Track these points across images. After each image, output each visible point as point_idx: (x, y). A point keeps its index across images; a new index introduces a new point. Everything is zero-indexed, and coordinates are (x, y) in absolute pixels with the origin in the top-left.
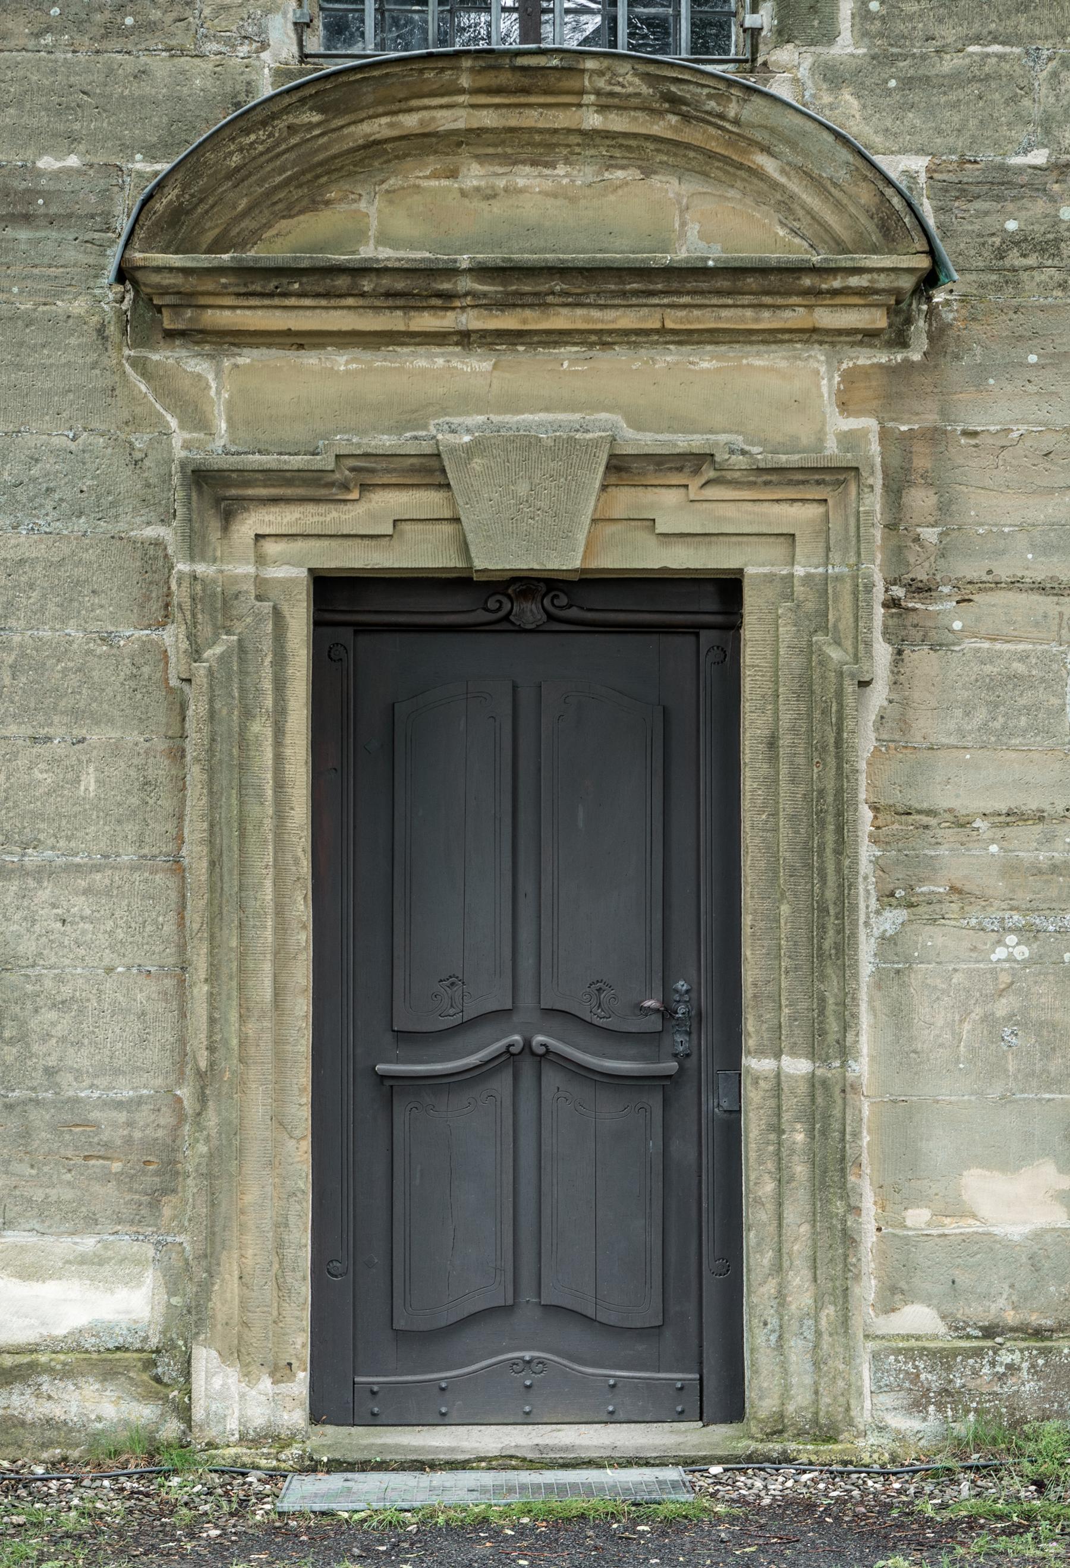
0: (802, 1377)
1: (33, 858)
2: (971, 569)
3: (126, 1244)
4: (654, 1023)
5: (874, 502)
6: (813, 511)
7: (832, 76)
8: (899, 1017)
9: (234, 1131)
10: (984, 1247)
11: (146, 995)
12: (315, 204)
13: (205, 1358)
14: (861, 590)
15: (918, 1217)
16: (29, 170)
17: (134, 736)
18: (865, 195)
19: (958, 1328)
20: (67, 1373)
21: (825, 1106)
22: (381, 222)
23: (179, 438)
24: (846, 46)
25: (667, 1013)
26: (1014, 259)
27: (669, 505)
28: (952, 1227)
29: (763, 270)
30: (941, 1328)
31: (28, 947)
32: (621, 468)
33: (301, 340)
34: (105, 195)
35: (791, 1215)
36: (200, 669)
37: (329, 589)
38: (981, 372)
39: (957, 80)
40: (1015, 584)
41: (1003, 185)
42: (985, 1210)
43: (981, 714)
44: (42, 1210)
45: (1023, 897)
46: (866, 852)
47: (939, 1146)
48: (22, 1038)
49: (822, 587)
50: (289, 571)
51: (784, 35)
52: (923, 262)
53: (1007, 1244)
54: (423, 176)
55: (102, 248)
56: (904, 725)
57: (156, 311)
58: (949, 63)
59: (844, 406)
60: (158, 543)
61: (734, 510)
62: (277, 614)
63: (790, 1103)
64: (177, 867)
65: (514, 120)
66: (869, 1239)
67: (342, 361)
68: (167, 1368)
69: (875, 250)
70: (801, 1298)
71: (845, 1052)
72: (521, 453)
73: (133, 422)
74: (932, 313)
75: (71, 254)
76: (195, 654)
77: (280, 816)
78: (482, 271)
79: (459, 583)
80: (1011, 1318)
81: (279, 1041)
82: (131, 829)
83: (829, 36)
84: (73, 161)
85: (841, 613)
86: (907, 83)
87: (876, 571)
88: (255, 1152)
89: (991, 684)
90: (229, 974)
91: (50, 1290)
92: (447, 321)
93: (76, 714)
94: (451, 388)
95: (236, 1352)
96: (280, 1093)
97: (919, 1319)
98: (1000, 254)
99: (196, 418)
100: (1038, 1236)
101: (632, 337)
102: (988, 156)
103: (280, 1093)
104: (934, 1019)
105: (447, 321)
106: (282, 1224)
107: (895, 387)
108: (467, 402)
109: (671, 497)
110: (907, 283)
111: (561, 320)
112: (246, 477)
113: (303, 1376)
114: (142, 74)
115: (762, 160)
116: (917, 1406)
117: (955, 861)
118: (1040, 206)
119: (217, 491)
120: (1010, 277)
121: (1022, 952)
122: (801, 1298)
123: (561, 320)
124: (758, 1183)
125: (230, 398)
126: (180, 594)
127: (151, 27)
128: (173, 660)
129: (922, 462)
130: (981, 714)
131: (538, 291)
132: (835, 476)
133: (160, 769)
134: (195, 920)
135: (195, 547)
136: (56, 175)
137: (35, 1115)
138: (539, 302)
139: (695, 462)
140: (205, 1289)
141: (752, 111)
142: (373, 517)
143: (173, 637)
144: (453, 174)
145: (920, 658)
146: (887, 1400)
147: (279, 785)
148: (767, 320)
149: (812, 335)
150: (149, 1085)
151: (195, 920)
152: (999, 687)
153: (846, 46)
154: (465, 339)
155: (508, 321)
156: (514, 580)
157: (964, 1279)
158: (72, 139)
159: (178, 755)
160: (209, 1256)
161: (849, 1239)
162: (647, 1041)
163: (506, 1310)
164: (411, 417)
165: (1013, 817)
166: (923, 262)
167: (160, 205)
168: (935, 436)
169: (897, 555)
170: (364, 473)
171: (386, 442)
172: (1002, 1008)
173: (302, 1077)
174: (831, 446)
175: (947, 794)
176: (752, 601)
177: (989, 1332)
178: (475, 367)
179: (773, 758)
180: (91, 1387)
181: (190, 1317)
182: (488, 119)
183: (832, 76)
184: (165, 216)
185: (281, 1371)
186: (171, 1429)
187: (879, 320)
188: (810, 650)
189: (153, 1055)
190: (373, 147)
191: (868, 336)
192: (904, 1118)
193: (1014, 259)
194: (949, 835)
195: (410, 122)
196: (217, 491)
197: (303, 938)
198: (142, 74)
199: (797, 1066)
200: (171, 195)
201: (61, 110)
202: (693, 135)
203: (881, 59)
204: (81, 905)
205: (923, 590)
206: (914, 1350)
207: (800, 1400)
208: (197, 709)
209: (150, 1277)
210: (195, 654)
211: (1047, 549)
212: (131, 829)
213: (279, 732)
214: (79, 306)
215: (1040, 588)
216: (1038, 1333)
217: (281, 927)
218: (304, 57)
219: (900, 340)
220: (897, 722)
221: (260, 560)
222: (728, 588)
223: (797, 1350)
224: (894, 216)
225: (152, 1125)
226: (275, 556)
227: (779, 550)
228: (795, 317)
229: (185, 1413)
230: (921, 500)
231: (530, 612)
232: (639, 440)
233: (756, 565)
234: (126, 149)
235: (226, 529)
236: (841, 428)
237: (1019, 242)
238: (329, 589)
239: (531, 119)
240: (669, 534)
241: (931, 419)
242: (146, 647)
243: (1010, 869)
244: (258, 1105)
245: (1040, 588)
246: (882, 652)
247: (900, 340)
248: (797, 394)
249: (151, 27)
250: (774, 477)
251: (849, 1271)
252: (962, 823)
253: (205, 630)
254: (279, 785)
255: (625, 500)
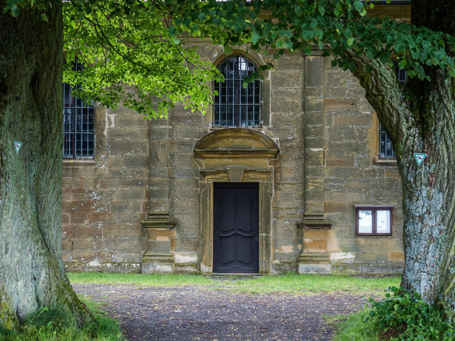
0: (264, 268)
1: (184, 212)
2: (283, 182)
3: (194, 253)
4: (250, 230)
5: (273, 175)
6: (266, 176)
7: (269, 129)
8: (275, 230)
9: (205, 241)
10: (284, 254)
11: (196, 227)
12: (214, 143)
13: (202, 264)
14: (271, 184)
15: (277, 251)
16: (184, 140)
17: (195, 200)
18: (271, 143)
19: (281, 262)
20: (188, 266)
21: (267, 239)
22: (221, 146)
23: (199, 168)
24: (270, 126)
25: (251, 229)
26: (288, 149)
27: (251, 175)
28: (280, 252)
29: (261, 151)
30: (279, 262)
31: (183, 222)
32: (246, 171)
33: (212, 158)
34: (192, 142)
35: (263, 250)
36: (202, 192)
37: (215, 184)
38: (284, 161)
39: (283, 129)
40: (288, 184)
41: (287, 141)
42: (284, 250)
43: (284, 198)
44: (185, 249)
45: (289, 217)
46: (272, 212)
47: (279, 243)
48: (183, 231)
49: (267, 184)
50: (211, 182)
51: (264, 125)
52: (277, 150)
53: (286, 253)
54: (225, 140)
55: (191, 148)
56: (276, 199)
57: (197, 155)
58: (281, 128)
59: (270, 165)
60: (197, 179)
61: (258, 176)
62: (210, 187)
63: (263, 238)
64: (199, 213)
65: (235, 135)
66: (272, 253)
67: (217, 160)
68: (198, 265)
69: (273, 149)
70: (264, 259)
71: (269, 233)
72: (235, 169)
73: (195, 166)
74: (279, 155)
75: (188, 149)
76: (201, 191)
77: (210, 208)
78: (231, 151)
79: (229, 183)
80: (287, 261)
81: (210, 232)
82: (194, 209)
83: (269, 125)
84: (188, 139)
85: (269, 187)
86: (277, 130)
87: (273, 182)
88: (207, 243)
89: (285, 194)
90: (204, 225)
91: (186, 257)
92: (228, 156)
93: (189, 197)
94: (228, 162)
95: (205, 264)
96: (210, 237)
97: (277, 261)
98: (287, 148)
99: (201, 166)
100: (290, 253)
101: (247, 158)
102: (286, 138)
103: (210, 237)
104: (279, 230)
105: (228, 156)
106: (210, 251)
107: (275, 163)
108: (230, 164)
109: (251, 174)
110: (276, 152)
111: (239, 156)
112: (206, 172)
113: (212, 267)
114: (196, 129)
115: (261, 139)
116: (276, 270)
117: (281, 213)
118: (291, 143)
119: (203, 174)
120: (288, 151)
121: (288, 223)
122: (264, 259)
123: (239, 156)
124: (260, 247)
125: (205, 163)
126: (200, 185)
127: (197, 124)
128: (25, 82)
129: (278, 171)
130: (284, 198)
131: (237, 153)
132: (268, 172)
133: (197, 203)
134: (201, 219)
135: (201, 180)
136: (186, 140)
137: (184, 239)
138: (237, 154)
139: (253, 171)
140: (202, 257)
141: (259, 134)
142: (220, 176)
143: (199, 189)
144: (228, 140)
145: (278, 192)
146: (273, 270)
147: (210, 205)
148: (261, 156)
149: (266, 157)
150: (196, 236)
151: (201, 219)
152: (286, 195)
153: (270, 126)
154: (230, 158)
155: (234, 156)
156: (380, 121)
157: (282, 257)
158: (188, 136)
159: (199, 201)
160: (202, 254)
161: (269, 253)
162: (249, 232)
163: (234, 261)
164: (224, 166)
165: (288, 208)
166: (277, 150)
167: (198, 144)
168: (280, 168)
169: (275, 181)
170: (219, 172)
171: (221, 169)
172: (286, 229)
173: (212, 235)
174: (268, 169)
175: (282, 205)
176: (260, 185)
177: (284, 263)
178: (231, 160)
179: (262, 202)
180: (190, 267)
181: (200, 260)
182: (232, 135)
183: (269, 129)
184: (198, 145)
185: (210, 266)
186: (198, 272)
187: (273, 156)
188: (266, 191)
189: (196, 233)
190: (220, 137)
191: (272, 157)
192: (276, 240)
193: (288, 149)
194: (281, 210)
195: (224, 135)
196: (203, 174)
197: (212, 221)
198: (196, 129)
199: (264, 235)
200: (199, 143)
201: (187, 133)
202: (254, 136)
203: (274, 127)
204: (189, 217)
205: (278, 184)
206: (276, 264)
207: (264, 269)
208: (201, 197)
209: (196, 256)
210: (201, 191)
211: (291, 180)
212: (194, 209)
213: (210, 199)
214: (189, 154)
215: (291, 184)
216: (290, 263)
217: (210, 220)
218: (213, 127)
219: (276, 157)
220: (275, 198)
221: (208, 181)
222: (258, 183)
223: (264, 265)
224: (274, 146)
225: (197, 240)
226: (209, 180)
227: (263, 180)
228: (264, 155)
229: (200, 270)
230: (278, 175)
231: (237, 186)
232: (248, 168)
233: (260, 181)
234: (194, 138)
235: (204, 178)
236: (270, 167)
237: (289, 147)
238: (215, 184)
239: (236, 135)
240: (251, 178)
241: (279, 166)
242: (196, 190)
243: (287, 214)
244: (207, 238)
245: (291, 184)
246: (274, 191)
247: (276, 157)
248: (265, 163)
249: (197, 124)
250: (262, 172)
251: (269, 256)
252: (282, 209)
253: (202, 189)
254: (210, 205)
255: (246, 175)
